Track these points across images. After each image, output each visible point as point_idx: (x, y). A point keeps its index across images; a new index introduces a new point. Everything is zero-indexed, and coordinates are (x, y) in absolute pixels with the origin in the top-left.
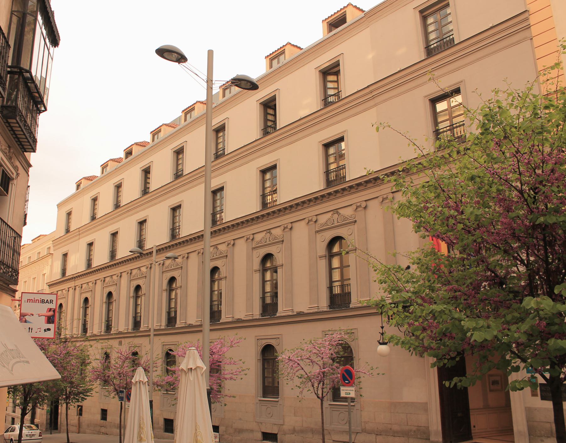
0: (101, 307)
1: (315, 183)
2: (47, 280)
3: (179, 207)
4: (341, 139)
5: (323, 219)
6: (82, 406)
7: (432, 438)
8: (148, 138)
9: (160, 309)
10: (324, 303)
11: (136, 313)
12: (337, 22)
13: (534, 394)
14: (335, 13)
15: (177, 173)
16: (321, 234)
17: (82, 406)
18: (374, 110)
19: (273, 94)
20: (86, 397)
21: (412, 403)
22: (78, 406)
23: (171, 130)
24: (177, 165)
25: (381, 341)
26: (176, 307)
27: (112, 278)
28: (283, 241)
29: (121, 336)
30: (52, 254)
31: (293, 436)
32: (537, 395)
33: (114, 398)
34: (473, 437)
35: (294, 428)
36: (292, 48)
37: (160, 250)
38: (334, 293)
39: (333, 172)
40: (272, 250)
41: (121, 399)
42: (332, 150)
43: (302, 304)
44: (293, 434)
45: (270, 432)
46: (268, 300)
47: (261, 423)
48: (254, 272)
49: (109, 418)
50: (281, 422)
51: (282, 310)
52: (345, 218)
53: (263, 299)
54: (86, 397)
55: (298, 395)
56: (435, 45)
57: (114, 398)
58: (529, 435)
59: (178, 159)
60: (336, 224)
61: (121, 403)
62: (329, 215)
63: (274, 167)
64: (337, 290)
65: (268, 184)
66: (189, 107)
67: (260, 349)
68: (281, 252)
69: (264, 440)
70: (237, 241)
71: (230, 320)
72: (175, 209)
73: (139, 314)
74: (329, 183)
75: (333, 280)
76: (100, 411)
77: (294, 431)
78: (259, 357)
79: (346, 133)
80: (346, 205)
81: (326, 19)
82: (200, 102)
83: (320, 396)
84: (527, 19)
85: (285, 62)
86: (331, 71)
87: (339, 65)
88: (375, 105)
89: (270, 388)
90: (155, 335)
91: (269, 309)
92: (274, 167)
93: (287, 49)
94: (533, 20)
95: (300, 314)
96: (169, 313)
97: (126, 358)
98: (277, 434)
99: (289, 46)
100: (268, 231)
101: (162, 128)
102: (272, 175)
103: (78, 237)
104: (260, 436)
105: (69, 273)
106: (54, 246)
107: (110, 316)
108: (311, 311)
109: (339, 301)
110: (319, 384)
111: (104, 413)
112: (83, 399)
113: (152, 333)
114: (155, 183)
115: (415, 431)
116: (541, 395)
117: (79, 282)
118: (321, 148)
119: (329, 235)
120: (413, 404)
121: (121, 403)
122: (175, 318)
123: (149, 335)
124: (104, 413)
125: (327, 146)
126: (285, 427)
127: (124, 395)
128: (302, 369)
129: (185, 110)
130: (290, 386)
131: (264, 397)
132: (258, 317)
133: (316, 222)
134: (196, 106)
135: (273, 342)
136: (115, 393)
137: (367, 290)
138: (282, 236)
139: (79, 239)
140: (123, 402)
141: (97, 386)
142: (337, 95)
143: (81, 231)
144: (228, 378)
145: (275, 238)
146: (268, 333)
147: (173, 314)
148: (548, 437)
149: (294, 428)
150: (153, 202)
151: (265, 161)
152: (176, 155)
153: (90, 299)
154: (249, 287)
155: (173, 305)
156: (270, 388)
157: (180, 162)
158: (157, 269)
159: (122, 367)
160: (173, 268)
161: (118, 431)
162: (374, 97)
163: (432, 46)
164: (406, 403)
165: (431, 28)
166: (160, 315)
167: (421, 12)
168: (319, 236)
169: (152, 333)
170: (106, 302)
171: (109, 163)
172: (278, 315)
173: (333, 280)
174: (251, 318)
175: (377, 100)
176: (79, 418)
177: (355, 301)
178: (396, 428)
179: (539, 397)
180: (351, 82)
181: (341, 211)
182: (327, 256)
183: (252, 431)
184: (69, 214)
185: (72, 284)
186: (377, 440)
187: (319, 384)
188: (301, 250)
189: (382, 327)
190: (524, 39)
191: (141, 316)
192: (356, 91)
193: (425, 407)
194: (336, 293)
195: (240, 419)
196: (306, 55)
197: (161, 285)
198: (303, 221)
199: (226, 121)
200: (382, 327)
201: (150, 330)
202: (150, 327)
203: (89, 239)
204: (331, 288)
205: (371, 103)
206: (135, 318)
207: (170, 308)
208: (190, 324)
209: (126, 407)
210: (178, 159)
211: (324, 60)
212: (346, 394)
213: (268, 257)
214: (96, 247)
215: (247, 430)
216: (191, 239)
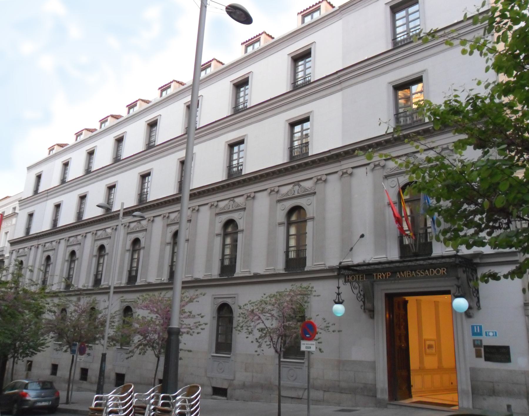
0: (63, 265)
2: (10, 237)
3: (149, 174)
4: (307, 120)
5: (284, 190)
6: (31, 362)
7: (379, 396)
8: (124, 112)
9: (121, 267)
11: (97, 271)
14: (310, 7)
15: (149, 144)
16: (281, 204)
17: (31, 362)
18: (339, 94)
19: (246, 76)
20: (36, 352)
22: (28, 361)
23: (146, 106)
25: (337, 301)
26: (137, 267)
28: (245, 209)
29: (80, 293)
30: (17, 214)
33: (66, 351)
34: (413, 396)
36: (267, 37)
37: (128, 212)
38: (290, 257)
39: (297, 148)
40: (235, 216)
41: (73, 352)
42: (297, 128)
43: (259, 267)
46: (227, 262)
47: (212, 378)
49: (59, 373)
50: (231, 377)
51: (239, 271)
52: (306, 190)
53: (222, 260)
54: (36, 352)
55: (256, 349)
56: (402, 38)
57: (66, 351)
58: (473, 393)
59: (151, 132)
60: (296, 194)
61: (73, 356)
62: (291, 186)
66: (166, 85)
67: (216, 307)
68: (242, 219)
69: (213, 394)
71: (189, 279)
72: (144, 176)
73: (100, 272)
74: (292, 158)
75: (290, 245)
76: (50, 366)
77: (244, 386)
78: (216, 315)
79: (312, 113)
80: (307, 179)
81: (301, 12)
82: (176, 81)
83: (279, 350)
85: (260, 48)
86: (302, 56)
88: (341, 90)
89: (224, 345)
90: (115, 293)
91: (228, 269)
93: (263, 37)
95: (256, 276)
96: (130, 272)
97: (83, 312)
99: (264, 35)
100: (232, 199)
101: (138, 103)
105: (33, 232)
106: (20, 206)
107: (71, 273)
108: (268, 273)
109: (295, 264)
110: (278, 338)
111: (55, 368)
112: (33, 354)
113: (112, 290)
116: (485, 356)
117: (42, 241)
118: (287, 126)
120: (360, 363)
121: (73, 356)
122: (136, 277)
123: (109, 292)
124: (55, 368)
125: (293, 125)
126: (236, 382)
127: (77, 348)
128: (263, 322)
129: (162, 87)
130: (243, 342)
131: (216, 353)
132: (216, 277)
135: (229, 301)
136: (68, 346)
137: (326, 250)
138: (244, 204)
139: (47, 200)
140: (75, 356)
141: (50, 339)
143: (50, 192)
144: (185, 333)
145: (238, 205)
146: (224, 292)
147: (134, 274)
148: (490, 396)
151: (233, 136)
153: (52, 257)
154: (210, 250)
155: (135, 265)
156: (224, 345)
158: (122, 231)
159: (78, 320)
160: (138, 229)
161: (67, 386)
162: (340, 83)
163: (399, 39)
164: (354, 362)
165: (398, 23)
166: (121, 273)
168: (279, 205)
169: (112, 290)
171: (84, 132)
172: (235, 275)
173: (290, 245)
174: (209, 278)
175: (343, 85)
176: (27, 374)
177: (310, 265)
178: (343, 385)
179: (483, 359)
180: (320, 67)
181: (302, 184)
182: (286, 223)
184: (39, 177)
185: (35, 243)
186: (325, 396)
187: (278, 338)
188: (262, 215)
189: (338, 288)
191: (102, 274)
192: (324, 76)
193: (373, 366)
194: (292, 257)
195: (192, 374)
197: (124, 244)
200: (338, 288)
201: (109, 288)
202: (110, 284)
203: (56, 200)
204: (287, 253)
205: (338, 87)
206: (96, 276)
207: (131, 267)
208: (149, 283)
209: (78, 360)
210: (151, 132)
212: (307, 347)
213: (230, 223)
214: (63, 209)
216: (158, 204)
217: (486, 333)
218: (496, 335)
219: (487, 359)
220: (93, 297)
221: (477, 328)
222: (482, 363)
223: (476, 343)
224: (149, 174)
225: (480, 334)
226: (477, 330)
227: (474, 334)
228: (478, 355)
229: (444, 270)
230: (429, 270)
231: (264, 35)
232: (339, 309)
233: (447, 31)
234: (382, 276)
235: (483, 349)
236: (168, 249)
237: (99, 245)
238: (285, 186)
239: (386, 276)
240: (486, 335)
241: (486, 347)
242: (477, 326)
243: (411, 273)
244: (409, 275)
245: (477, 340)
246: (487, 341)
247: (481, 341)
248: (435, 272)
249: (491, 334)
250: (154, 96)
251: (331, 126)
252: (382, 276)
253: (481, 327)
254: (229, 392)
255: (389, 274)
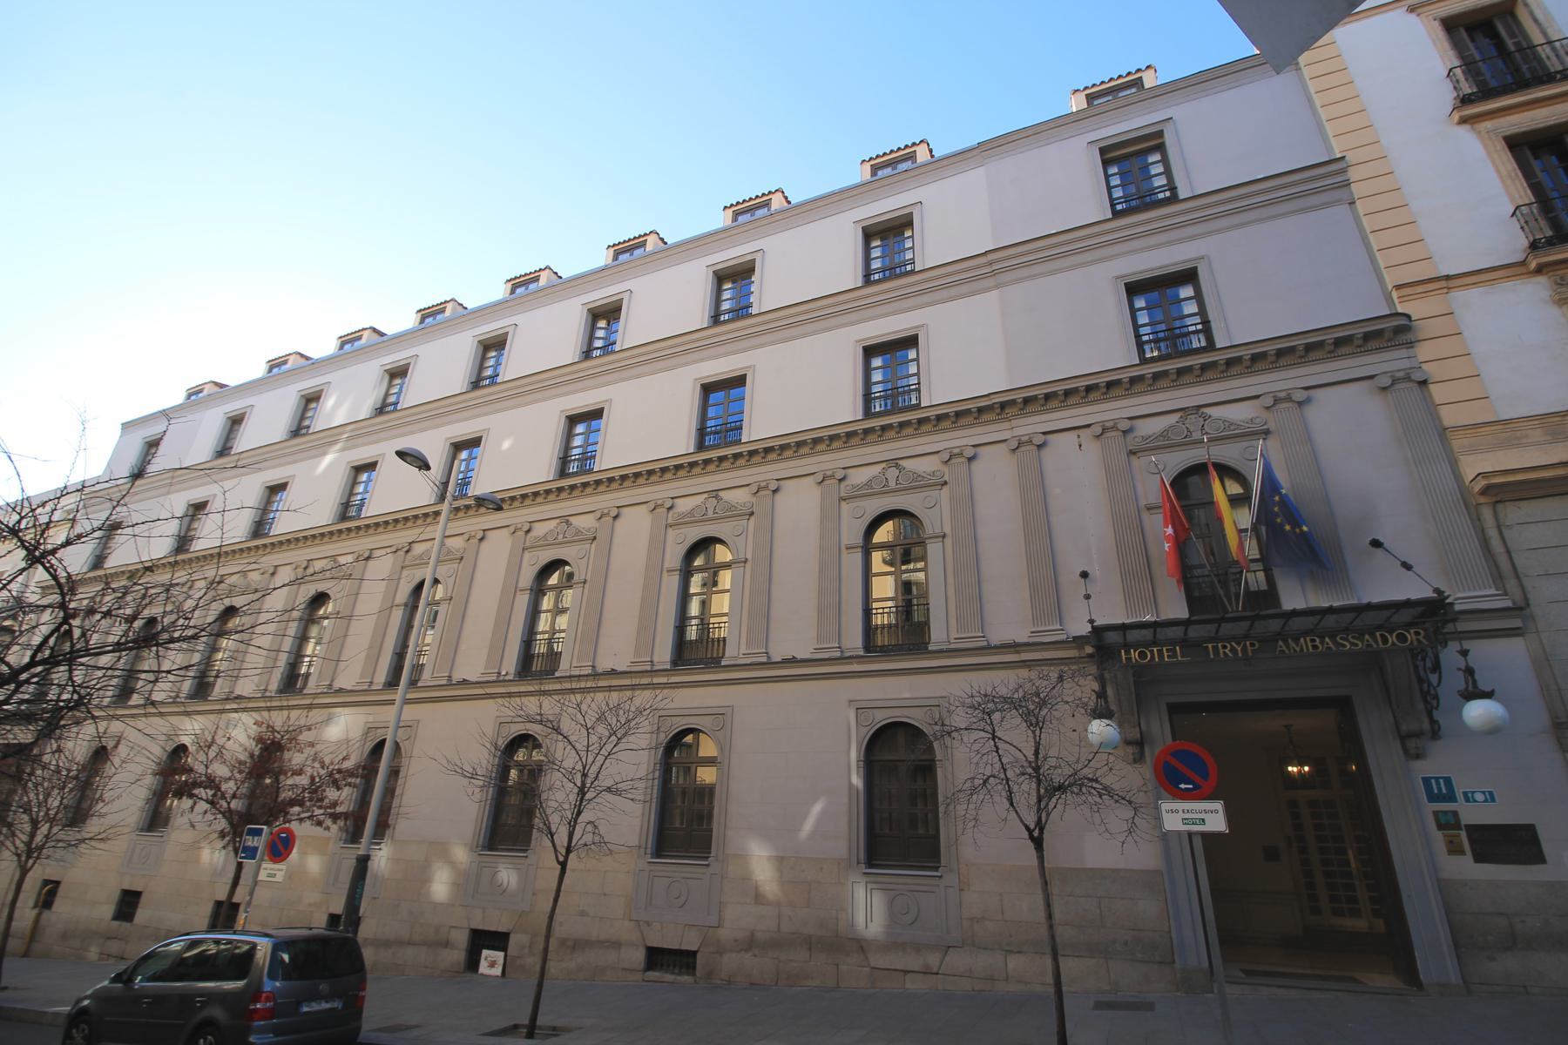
1: (541, 470)
10: (663, 653)
12: (626, 249)
13: (1454, 849)
18: (995, 293)
19: (749, 258)
21: (1114, 871)
24: (302, 418)
27: (245, 577)
31: (748, 955)
32: (1462, 852)
35: (752, 934)
44: (746, 951)
45: (493, 929)
47: (648, 923)
48: (665, 574)
60: (710, 514)
61: (240, 866)
62: (877, 469)
63: (597, 414)
64: (692, 633)
65: (578, 441)
70: (489, 533)
84: (1344, 171)
86: (608, 313)
87: (753, 270)
88: (997, 287)
92: (597, 414)
94: (1353, 174)
98: (694, 953)
102: (588, 428)
103: (163, 490)
104: (639, 956)
114: (245, 441)
115: (1126, 943)
116: (1473, 850)
119: (695, 534)
120: (1115, 874)
121: (240, 866)
126: (724, 934)
133: (669, 509)
134: (291, 359)
142: (396, 404)
149: (752, 934)
150: (831, 322)
152: (387, 377)
154: (503, 621)
157: (310, 414)
165: (726, 295)
167: (1103, 151)
170: (406, 605)
176: (39, 914)
179: (1469, 857)
181: (1208, 411)
183: (616, 944)
190: (1338, 202)
195: (583, 913)
196: (466, 317)
198: (1003, 445)
199: (626, 297)
209: (262, 876)
211: (600, 295)
215: (600, 943)
217: (1465, 794)
218: (1493, 800)
219: (1479, 858)
220: (174, 720)
221: (1438, 783)
222: (1465, 868)
223: (1443, 819)
224: (282, 487)
225: (1451, 797)
226: (1439, 789)
227: (1433, 798)
228: (1454, 849)
229: (1417, 633)
230: (1372, 635)
231: (653, 236)
232: (1100, 729)
233: (991, 257)
234: (1233, 650)
235: (1463, 834)
236: (398, 616)
237: (312, 593)
238: (689, 494)
239: (1244, 650)
240: (1467, 800)
241: (1472, 830)
242: (1437, 779)
243: (1322, 642)
244: (1315, 647)
245: (1445, 813)
246: (1472, 814)
247: (1455, 813)
248: (1392, 639)
249: (1479, 797)
250: (328, 347)
251: (966, 354)
252: (1233, 650)
253: (1448, 781)
254: (700, 960)
255: (1252, 645)
